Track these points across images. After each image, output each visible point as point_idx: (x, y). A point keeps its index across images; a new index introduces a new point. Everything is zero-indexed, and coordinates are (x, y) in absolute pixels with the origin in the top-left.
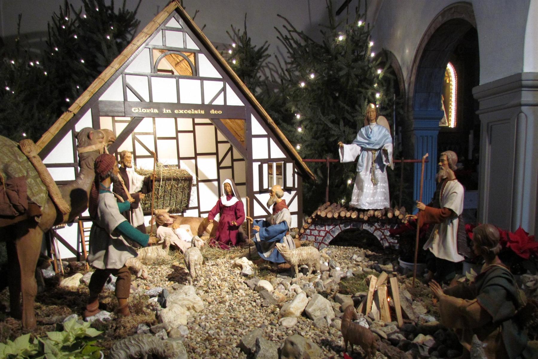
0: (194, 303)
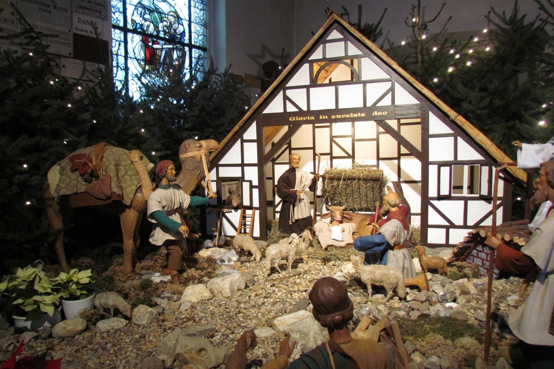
0: (222, 289)
